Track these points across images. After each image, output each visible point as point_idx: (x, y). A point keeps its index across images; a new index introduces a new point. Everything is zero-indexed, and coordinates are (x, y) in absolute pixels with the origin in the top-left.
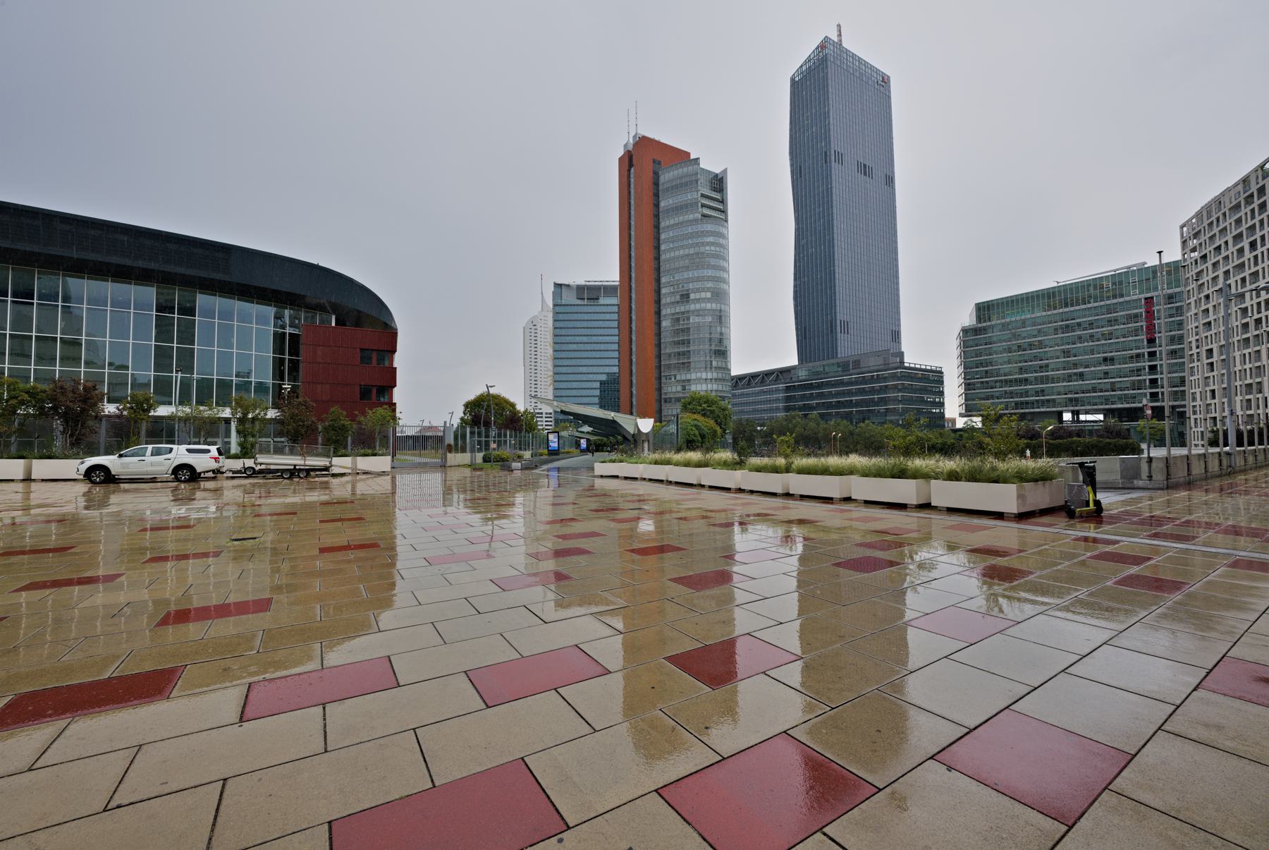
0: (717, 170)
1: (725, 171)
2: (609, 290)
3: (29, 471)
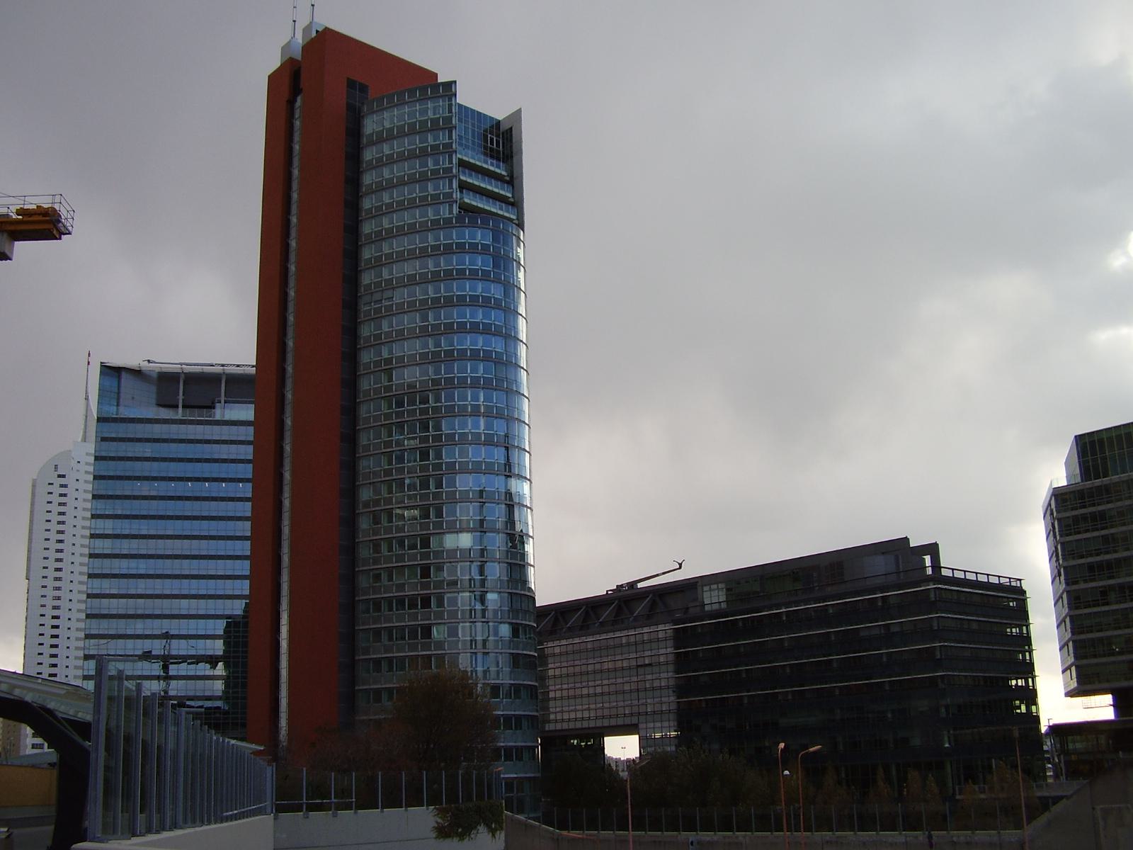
0: (498, 111)
1: (517, 115)
2: (230, 385)
3: (178, 672)
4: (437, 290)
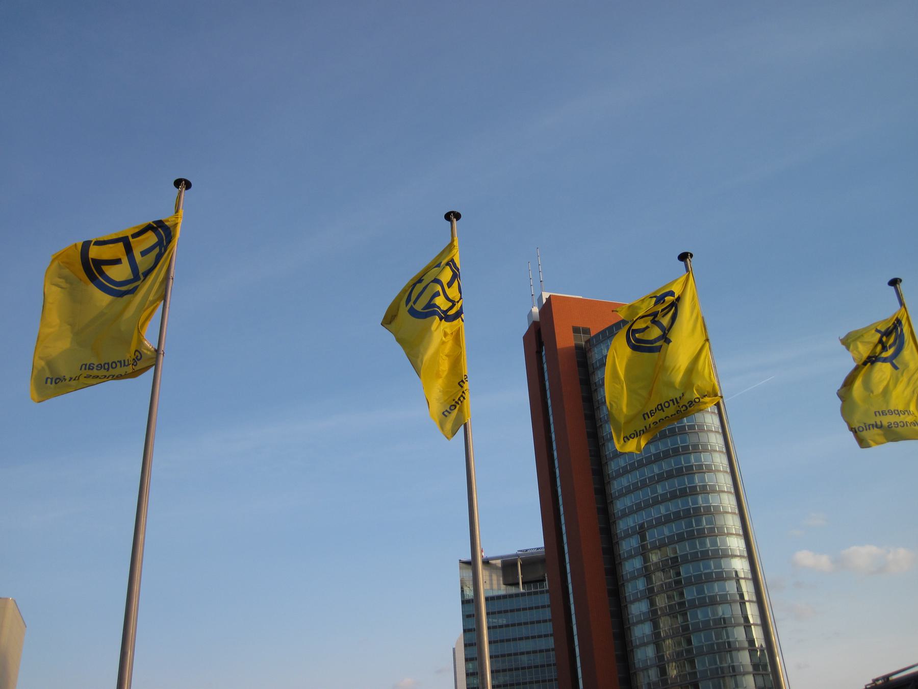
4: (660, 468)
